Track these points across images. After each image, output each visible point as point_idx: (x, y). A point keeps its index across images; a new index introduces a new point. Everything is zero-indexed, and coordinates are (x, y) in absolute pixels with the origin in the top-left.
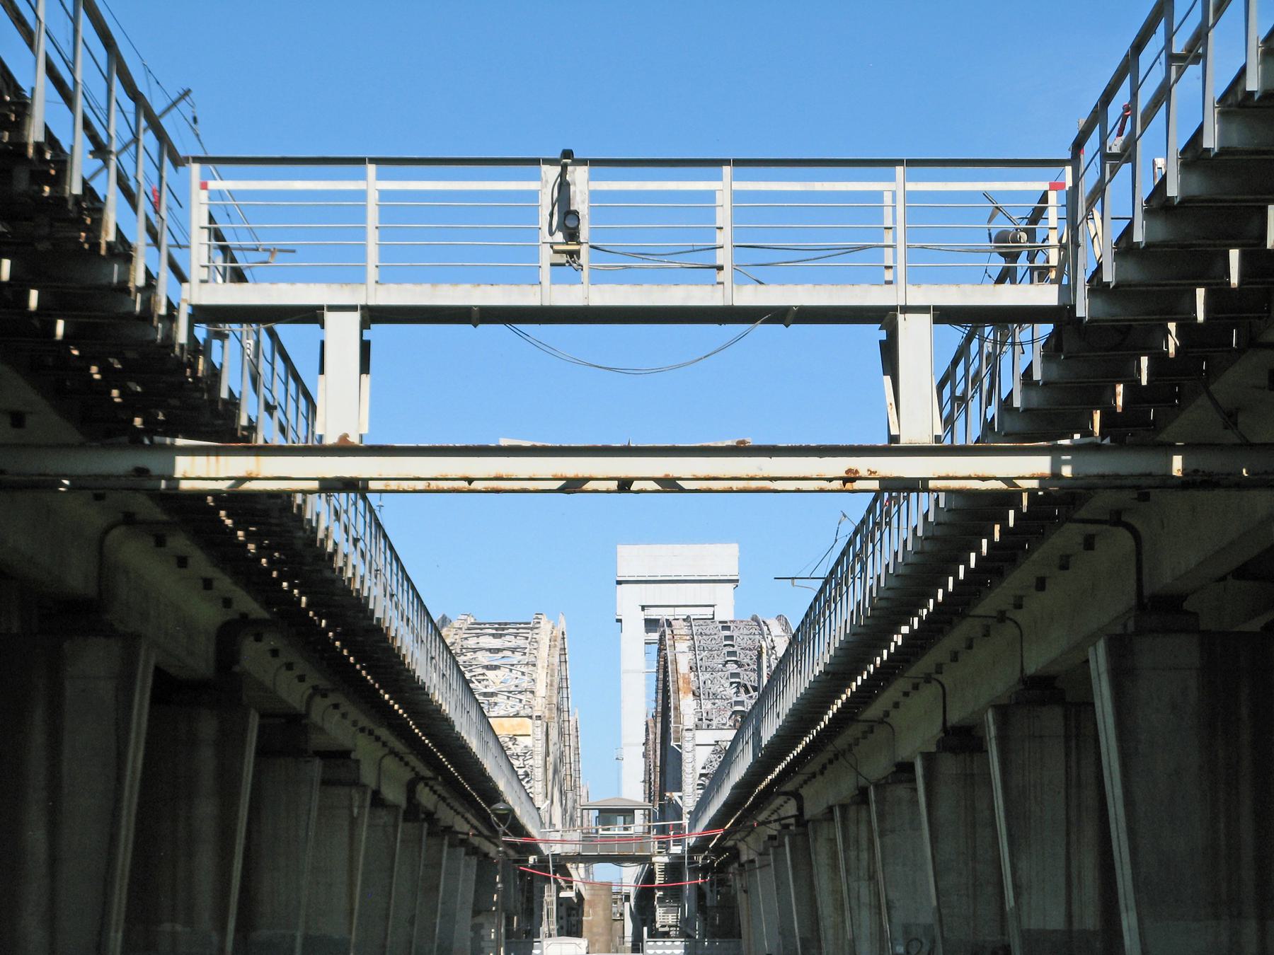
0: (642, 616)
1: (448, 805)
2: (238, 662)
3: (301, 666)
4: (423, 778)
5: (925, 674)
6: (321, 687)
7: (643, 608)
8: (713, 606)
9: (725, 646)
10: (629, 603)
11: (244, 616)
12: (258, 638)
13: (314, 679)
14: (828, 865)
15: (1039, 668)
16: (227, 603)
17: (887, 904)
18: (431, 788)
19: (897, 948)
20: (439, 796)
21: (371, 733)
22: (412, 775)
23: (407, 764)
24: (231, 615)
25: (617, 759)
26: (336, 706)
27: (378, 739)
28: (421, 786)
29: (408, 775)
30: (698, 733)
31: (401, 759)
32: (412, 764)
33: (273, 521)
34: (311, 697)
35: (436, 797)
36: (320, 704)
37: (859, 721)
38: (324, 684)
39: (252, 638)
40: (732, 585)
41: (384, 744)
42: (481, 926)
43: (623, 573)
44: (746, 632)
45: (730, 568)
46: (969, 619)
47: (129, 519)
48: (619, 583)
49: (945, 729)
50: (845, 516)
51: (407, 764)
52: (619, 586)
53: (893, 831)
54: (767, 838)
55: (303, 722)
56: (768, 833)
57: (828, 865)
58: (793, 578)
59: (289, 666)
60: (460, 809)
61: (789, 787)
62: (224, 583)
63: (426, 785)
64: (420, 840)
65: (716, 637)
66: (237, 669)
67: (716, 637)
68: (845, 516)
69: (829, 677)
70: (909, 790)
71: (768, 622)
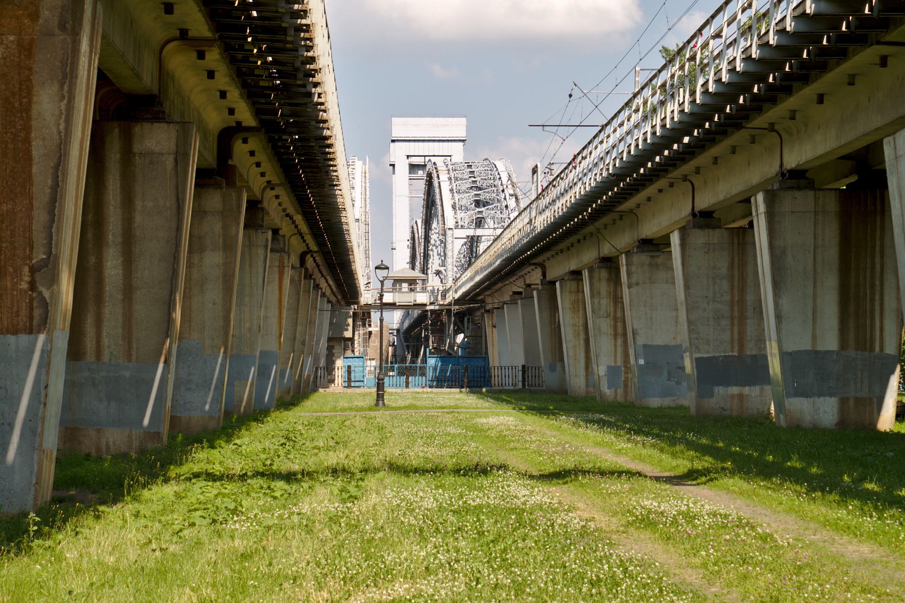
0: (406, 162)
1: (319, 270)
2: (231, 157)
3: (266, 166)
4: (311, 251)
5: (683, 175)
6: (272, 182)
7: (408, 157)
8: (450, 156)
9: (470, 177)
10: (399, 154)
11: (239, 123)
12: (245, 141)
13: (272, 176)
14: (570, 308)
15: (801, 163)
16: (231, 111)
17: (633, 332)
18: (314, 258)
19: (640, 361)
20: (317, 264)
21: (291, 218)
22: (305, 249)
23: (304, 241)
24: (231, 121)
25: (392, 249)
26: (277, 197)
27: (294, 222)
28: (309, 256)
29: (303, 248)
30: (455, 231)
31: (303, 238)
32: (307, 242)
33: (289, 39)
34: (264, 189)
35: (315, 264)
36: (270, 194)
37: (614, 212)
38: (275, 180)
39: (241, 141)
40: (461, 144)
41: (296, 227)
42: (333, 347)
43: (396, 134)
44: (482, 169)
45: (461, 133)
46: (744, 130)
47: (183, 35)
48: (393, 141)
49: (694, 214)
50: (575, 85)
51: (304, 241)
52: (392, 145)
53: (637, 284)
54: (512, 294)
55: (259, 206)
56: (513, 290)
57: (570, 308)
58: (543, 126)
59: (258, 165)
60: (325, 273)
61: (539, 260)
62: (235, 95)
63: (312, 256)
64: (309, 291)
65: (464, 172)
66: (230, 162)
67: (464, 172)
68: (575, 85)
69: (615, 178)
70: (649, 257)
71: (494, 162)
